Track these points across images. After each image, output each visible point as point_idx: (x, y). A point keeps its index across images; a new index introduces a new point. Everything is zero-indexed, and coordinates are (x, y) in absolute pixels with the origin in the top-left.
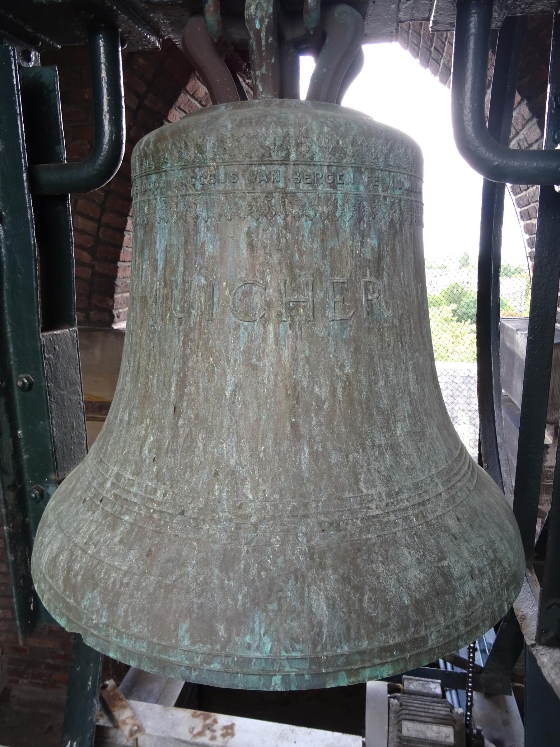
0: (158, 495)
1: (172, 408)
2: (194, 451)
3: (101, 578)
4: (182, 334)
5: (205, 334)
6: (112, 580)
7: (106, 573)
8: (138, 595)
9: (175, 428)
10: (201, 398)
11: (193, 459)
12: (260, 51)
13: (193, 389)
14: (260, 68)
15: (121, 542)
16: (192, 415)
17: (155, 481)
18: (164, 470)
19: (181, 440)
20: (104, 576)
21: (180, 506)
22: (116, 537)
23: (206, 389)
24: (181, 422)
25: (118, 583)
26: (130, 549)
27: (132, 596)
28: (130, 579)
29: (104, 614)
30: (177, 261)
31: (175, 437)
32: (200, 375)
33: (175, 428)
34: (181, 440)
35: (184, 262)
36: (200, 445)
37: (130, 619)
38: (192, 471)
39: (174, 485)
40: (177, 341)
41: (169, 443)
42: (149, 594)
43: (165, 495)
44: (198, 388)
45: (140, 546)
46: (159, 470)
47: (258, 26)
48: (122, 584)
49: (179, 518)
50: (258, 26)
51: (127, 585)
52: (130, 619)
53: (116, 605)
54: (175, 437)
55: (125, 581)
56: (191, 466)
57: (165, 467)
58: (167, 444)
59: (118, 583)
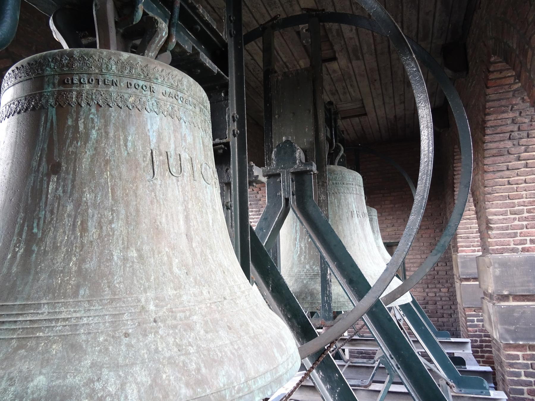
0: (205, 294)
1: (184, 236)
2: (208, 261)
3: (221, 357)
4: (180, 187)
5: (194, 188)
6: (229, 353)
7: (221, 352)
8: (249, 349)
9: (192, 249)
10: (200, 228)
11: (210, 266)
12: (157, 46)
13: (195, 222)
14: (152, 53)
15: (207, 332)
16: (199, 239)
17: (197, 286)
18: (198, 278)
19: (199, 256)
20: (222, 355)
21: (222, 295)
22: (199, 332)
23: (201, 222)
24: (194, 245)
25: (234, 351)
26: (217, 332)
27: (247, 352)
28: (237, 344)
29: (241, 375)
30: (169, 140)
31: (194, 255)
32: (196, 214)
33: (192, 249)
34: (199, 256)
35: (175, 142)
36: (210, 257)
37: (256, 365)
38: (214, 274)
39: (210, 285)
40: (177, 192)
41: (192, 260)
42: (253, 345)
43: (209, 293)
44: (197, 222)
45: (221, 327)
46: (195, 279)
47: (164, 35)
48: (236, 350)
49: (225, 302)
50: (164, 35)
51: (239, 348)
52: (256, 365)
53: (244, 363)
54: (194, 255)
55: (236, 347)
56: (212, 271)
57: (198, 276)
58: (191, 261)
59: (234, 351)
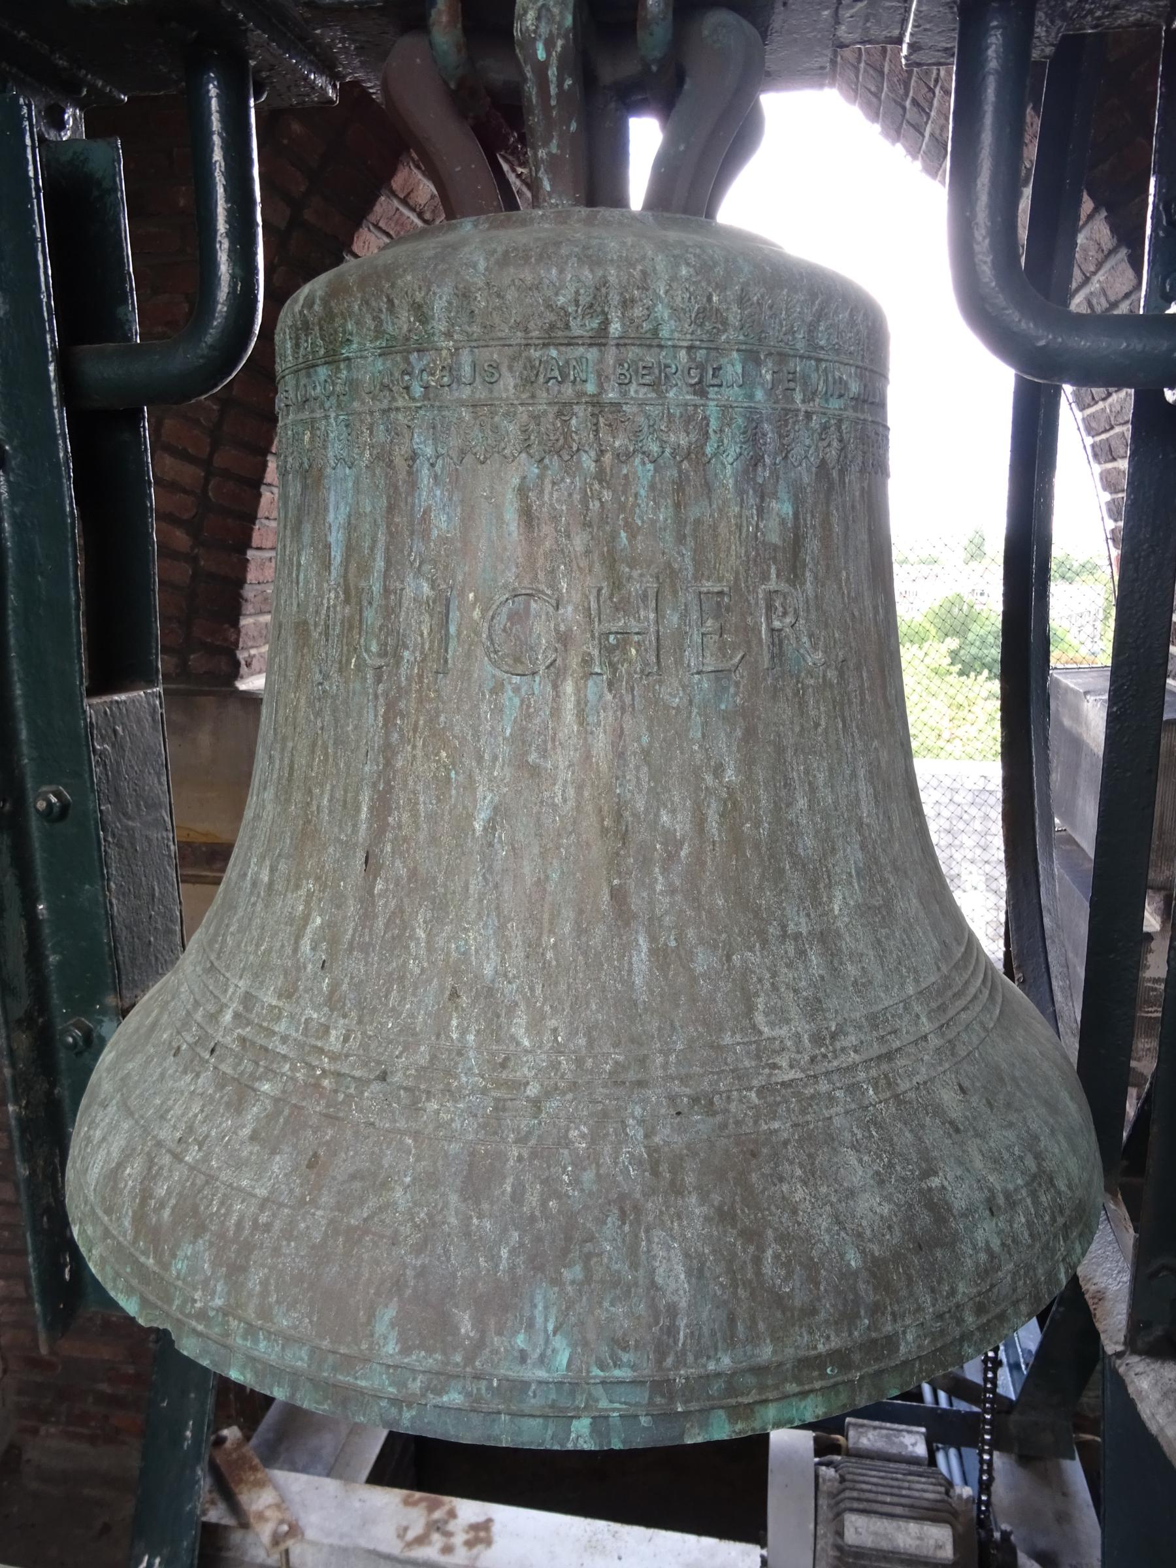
0: (332, 1039)
1: (361, 855)
2: (407, 947)
3: (212, 1214)
4: (381, 700)
5: (430, 701)
6: (234, 1218)
7: (222, 1203)
8: (289, 1248)
9: (367, 898)
10: (422, 836)
11: (405, 963)
12: (546, 108)
13: (405, 816)
14: (546, 144)
15: (254, 1137)
16: (403, 872)
17: (326, 1009)
18: (345, 987)
19: (380, 923)
20: (218, 1209)
21: (379, 1063)
22: (244, 1126)
23: (432, 817)
24: (379, 886)
25: (248, 1224)
26: (273, 1152)
27: (276, 1251)
28: (274, 1215)
29: (219, 1288)
30: (372, 549)
31: (367, 917)
32: (420, 787)
33: (367, 898)
34: (380, 923)
35: (387, 549)
36: (421, 934)
37: (273, 1298)
38: (403, 989)
39: (366, 1019)
40: (371, 716)
41: (355, 930)
42: (313, 1247)
43: (346, 1039)
44: (415, 815)
45: (295, 1146)
46: (335, 986)
47: (541, 55)
48: (255, 1225)
49: (376, 1087)
50: (541, 55)
51: (268, 1227)
52: (273, 1298)
53: (244, 1269)
54: (367, 917)
55: (263, 1219)
56: (402, 979)
57: (347, 980)
58: (350, 932)
59: (248, 1224)
